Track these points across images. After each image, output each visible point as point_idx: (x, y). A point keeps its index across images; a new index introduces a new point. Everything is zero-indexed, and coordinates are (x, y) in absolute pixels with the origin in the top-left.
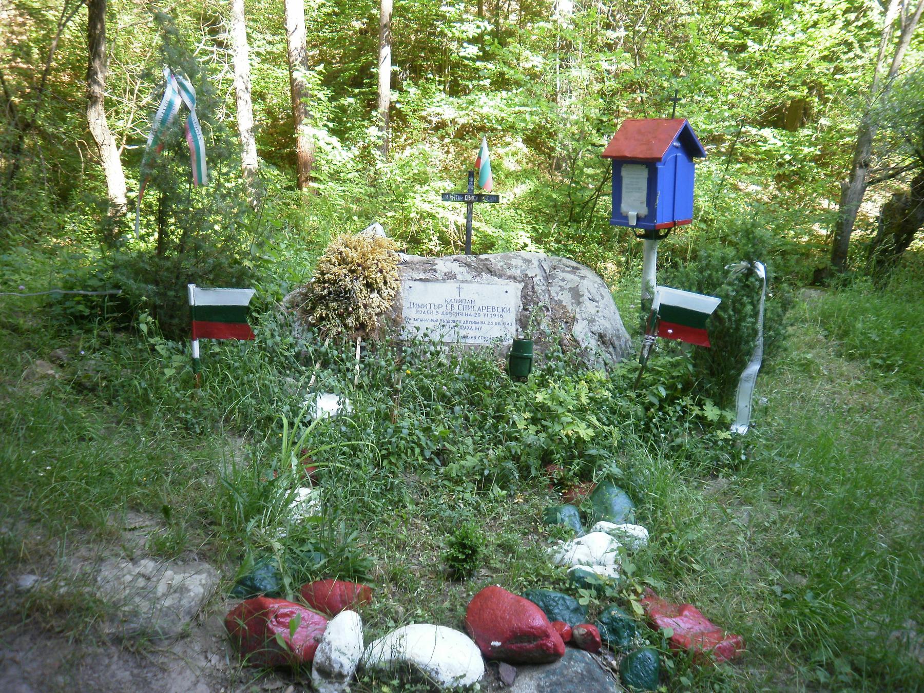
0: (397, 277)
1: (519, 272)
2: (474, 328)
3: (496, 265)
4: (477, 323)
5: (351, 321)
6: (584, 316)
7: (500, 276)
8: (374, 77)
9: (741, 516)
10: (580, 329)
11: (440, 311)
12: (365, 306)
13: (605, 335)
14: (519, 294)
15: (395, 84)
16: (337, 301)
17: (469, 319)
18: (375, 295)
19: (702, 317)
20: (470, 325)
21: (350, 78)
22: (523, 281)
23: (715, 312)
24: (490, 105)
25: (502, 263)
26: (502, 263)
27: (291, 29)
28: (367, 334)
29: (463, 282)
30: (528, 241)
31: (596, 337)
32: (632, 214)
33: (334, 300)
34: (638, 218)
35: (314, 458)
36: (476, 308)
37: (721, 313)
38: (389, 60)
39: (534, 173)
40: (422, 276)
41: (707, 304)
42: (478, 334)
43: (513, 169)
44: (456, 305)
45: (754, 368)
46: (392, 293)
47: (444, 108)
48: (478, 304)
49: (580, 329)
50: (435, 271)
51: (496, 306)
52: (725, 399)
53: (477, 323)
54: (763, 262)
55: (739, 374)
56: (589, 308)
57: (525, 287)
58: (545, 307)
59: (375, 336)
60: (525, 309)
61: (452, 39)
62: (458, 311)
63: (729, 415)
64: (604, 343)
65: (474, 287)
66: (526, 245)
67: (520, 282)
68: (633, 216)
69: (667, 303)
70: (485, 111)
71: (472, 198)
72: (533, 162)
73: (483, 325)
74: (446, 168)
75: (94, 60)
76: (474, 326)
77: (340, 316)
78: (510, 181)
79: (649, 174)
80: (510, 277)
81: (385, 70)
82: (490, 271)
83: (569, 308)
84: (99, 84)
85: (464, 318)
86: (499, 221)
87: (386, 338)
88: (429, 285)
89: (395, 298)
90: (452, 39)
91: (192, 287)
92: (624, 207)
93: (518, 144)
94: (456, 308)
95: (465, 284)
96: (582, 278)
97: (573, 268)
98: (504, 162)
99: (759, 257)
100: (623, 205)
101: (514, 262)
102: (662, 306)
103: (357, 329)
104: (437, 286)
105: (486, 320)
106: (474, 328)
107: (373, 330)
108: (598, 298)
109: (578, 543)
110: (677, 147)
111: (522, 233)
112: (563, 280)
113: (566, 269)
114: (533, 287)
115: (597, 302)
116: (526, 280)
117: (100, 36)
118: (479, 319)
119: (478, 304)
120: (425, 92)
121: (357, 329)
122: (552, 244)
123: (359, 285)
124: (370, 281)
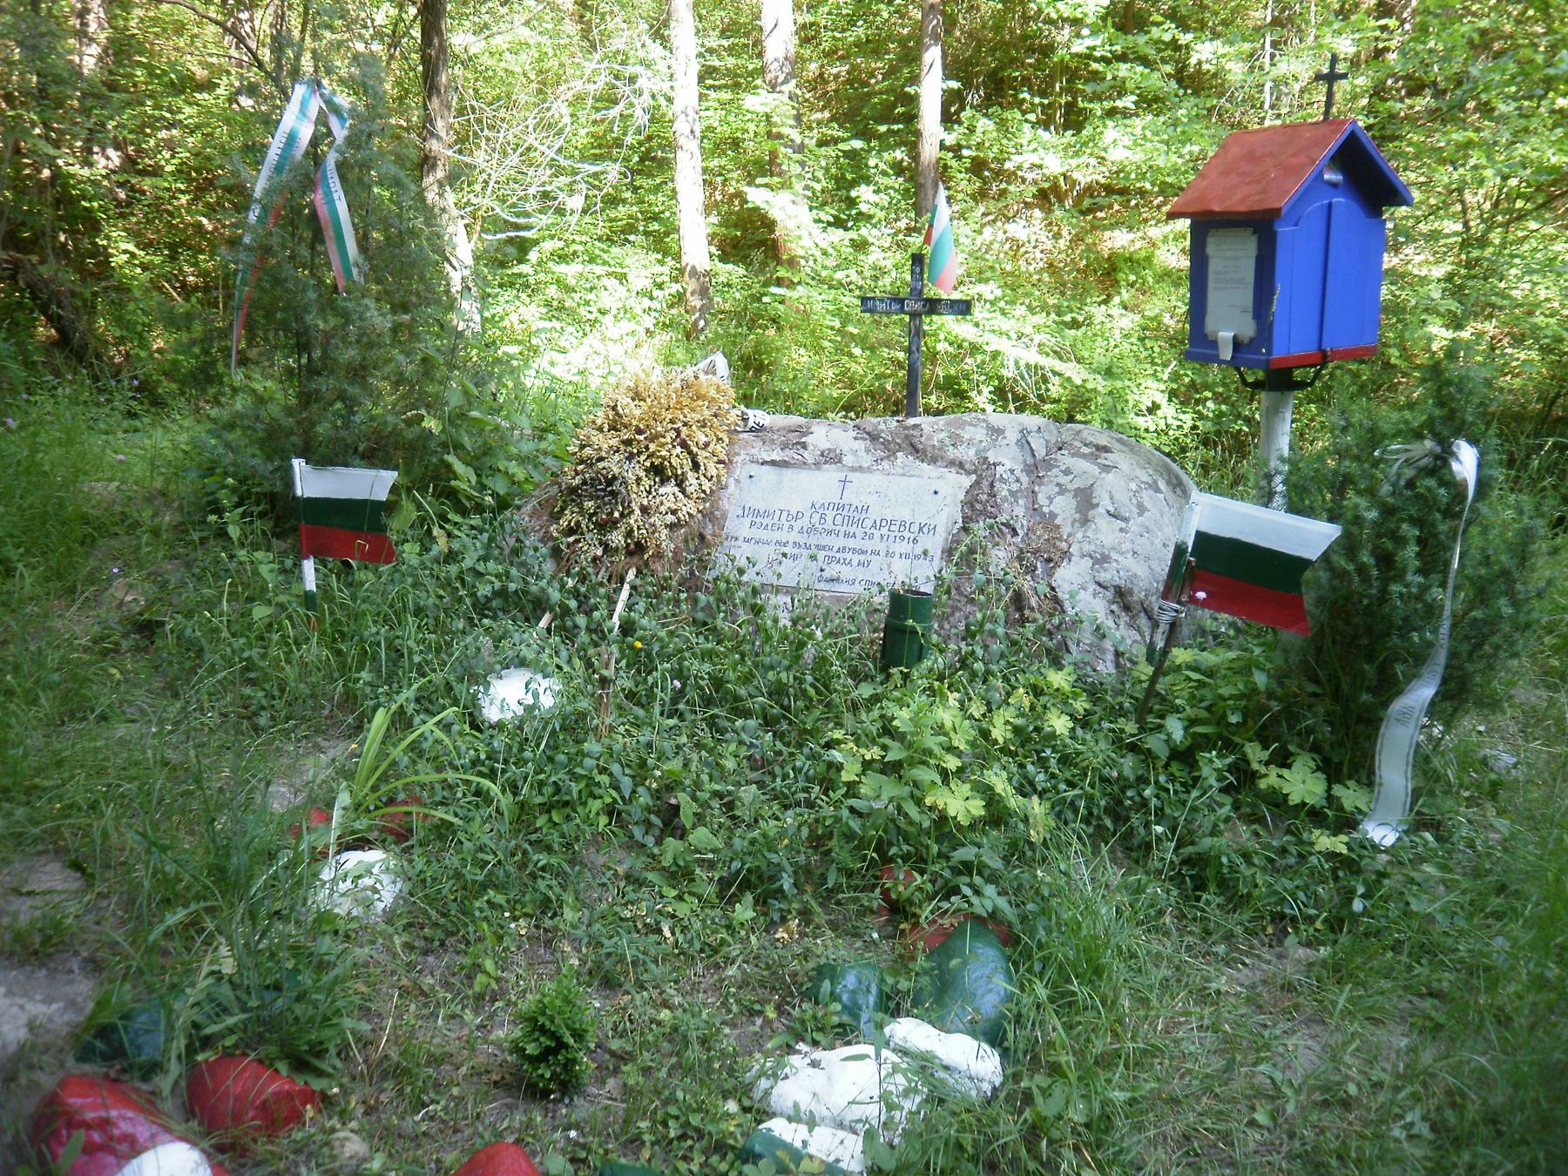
0: (723, 456)
1: (972, 452)
2: (855, 563)
3: (930, 438)
4: (864, 552)
5: (617, 538)
6: (1087, 548)
7: (933, 460)
8: (912, 100)
9: (1301, 1051)
10: (1070, 576)
11: (797, 525)
12: (645, 510)
13: (1130, 592)
17: (851, 543)
18: (670, 489)
19: (1296, 565)
20: (849, 556)
21: (868, 110)
22: (975, 472)
23: (1325, 556)
24: (1123, 145)
25: (942, 435)
26: (942, 435)
27: (767, 29)
28: (646, 564)
29: (853, 469)
30: (1162, 399)
31: (1110, 594)
32: (1226, 335)
34: (1237, 344)
35: (402, 796)
36: (868, 523)
38: (938, 70)
40: (776, 455)
41: (1309, 537)
42: (861, 574)
44: (830, 514)
45: (1423, 692)
47: (1040, 153)
49: (1070, 576)
51: (908, 519)
52: (1349, 758)
53: (864, 552)
54: (1473, 441)
55: (1386, 705)
56: (1105, 532)
57: (977, 483)
58: (1007, 525)
62: (831, 527)
63: (1350, 796)
64: (1127, 608)
65: (875, 480)
67: (969, 473)
69: (1213, 532)
70: (1117, 155)
71: (918, 306)
73: (874, 558)
74: (1051, 265)
75: (429, 97)
76: (856, 558)
79: (1259, 249)
80: (952, 463)
81: (932, 88)
82: (916, 450)
84: (439, 138)
85: (840, 542)
86: (1105, 361)
87: (691, 571)
88: (784, 470)
91: (298, 464)
92: (1210, 325)
94: (829, 519)
95: (858, 475)
96: (1107, 469)
98: (1157, 252)
99: (1462, 430)
101: (967, 433)
104: (804, 476)
105: (882, 547)
106: (855, 563)
108: (1129, 510)
109: (814, 1064)
110: (1334, 185)
111: (1150, 382)
112: (1067, 472)
113: (1085, 450)
114: (992, 485)
115: (1125, 520)
116: (983, 470)
117: (438, 58)
118: (868, 545)
119: (875, 514)
121: (630, 553)
122: (1210, 404)
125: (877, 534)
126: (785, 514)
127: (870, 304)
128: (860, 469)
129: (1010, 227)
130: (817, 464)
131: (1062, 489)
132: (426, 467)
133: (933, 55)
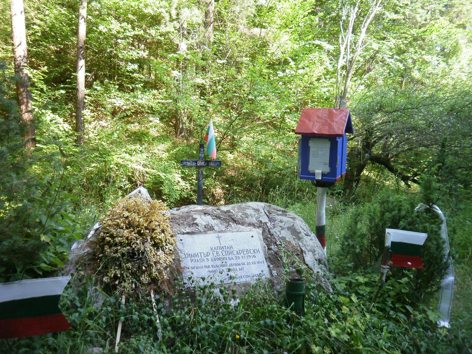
2: (238, 269)
3: (237, 216)
4: (239, 265)
7: (243, 224)
11: (210, 258)
12: (155, 263)
14: (261, 237)
15: (89, 85)
16: (130, 262)
18: (160, 252)
30: (180, 180)
33: (128, 261)
36: (235, 253)
37: (430, 244)
38: (83, 69)
39: (168, 138)
40: (188, 230)
43: (156, 135)
44: (220, 251)
46: (172, 248)
47: (118, 100)
48: (236, 248)
50: (197, 225)
57: (264, 231)
59: (165, 287)
60: (269, 249)
61: (122, 60)
65: (228, 235)
66: (179, 182)
68: (318, 173)
69: (394, 241)
72: (166, 131)
73: (244, 266)
76: (238, 267)
77: (133, 274)
78: (155, 143)
80: (250, 224)
81: (81, 75)
82: (235, 221)
83: (293, 243)
88: (195, 236)
89: (174, 252)
90: (122, 60)
93: (156, 120)
95: (222, 234)
97: (283, 211)
100: (309, 166)
102: (393, 243)
103: (149, 284)
105: (245, 261)
107: (163, 282)
111: (176, 175)
112: (281, 221)
114: (269, 231)
116: (261, 225)
118: (240, 261)
119: (236, 248)
120: (107, 90)
123: (149, 246)
124: (157, 241)
125: (240, 256)
126: (202, 254)
127: (185, 163)
128: (222, 231)
129: (101, 122)
130: (205, 232)
131: (283, 229)
132: (79, 275)
133: (82, 63)
